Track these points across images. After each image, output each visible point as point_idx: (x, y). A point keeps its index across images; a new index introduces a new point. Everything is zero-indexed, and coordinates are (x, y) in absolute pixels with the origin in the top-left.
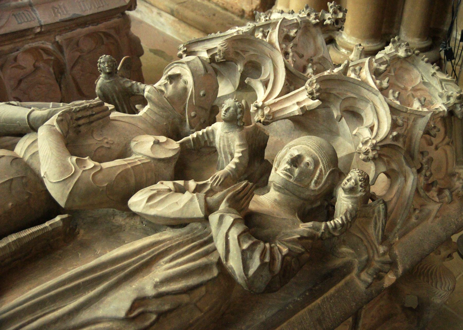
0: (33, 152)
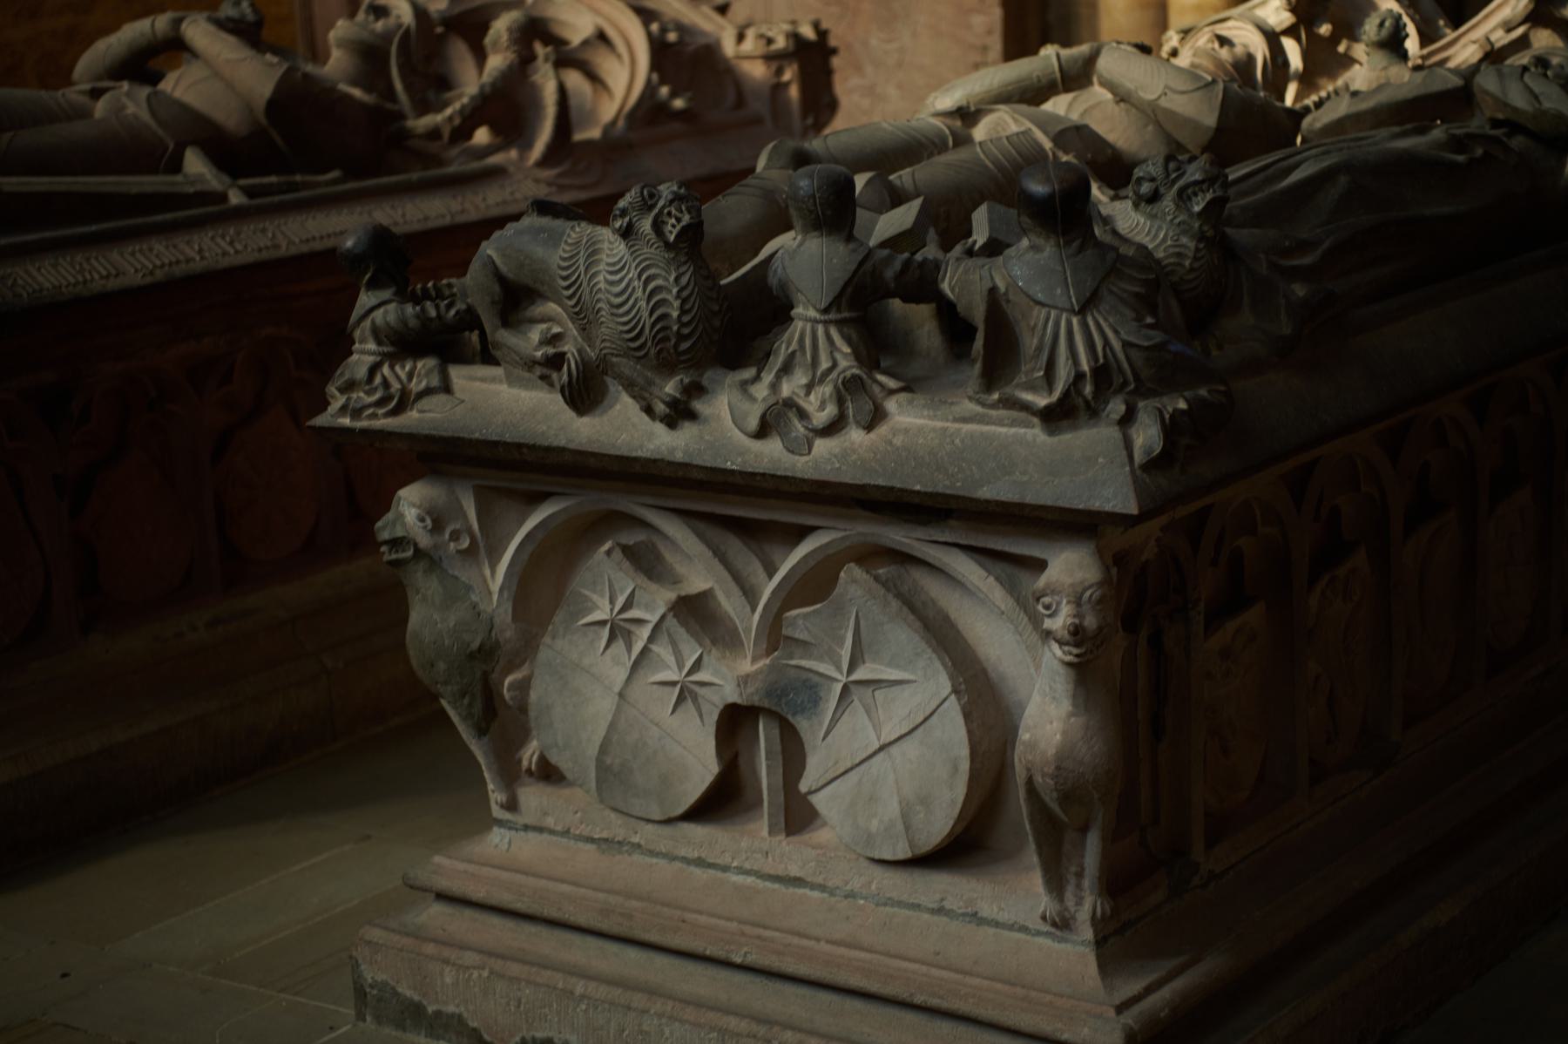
0: (1085, 106)
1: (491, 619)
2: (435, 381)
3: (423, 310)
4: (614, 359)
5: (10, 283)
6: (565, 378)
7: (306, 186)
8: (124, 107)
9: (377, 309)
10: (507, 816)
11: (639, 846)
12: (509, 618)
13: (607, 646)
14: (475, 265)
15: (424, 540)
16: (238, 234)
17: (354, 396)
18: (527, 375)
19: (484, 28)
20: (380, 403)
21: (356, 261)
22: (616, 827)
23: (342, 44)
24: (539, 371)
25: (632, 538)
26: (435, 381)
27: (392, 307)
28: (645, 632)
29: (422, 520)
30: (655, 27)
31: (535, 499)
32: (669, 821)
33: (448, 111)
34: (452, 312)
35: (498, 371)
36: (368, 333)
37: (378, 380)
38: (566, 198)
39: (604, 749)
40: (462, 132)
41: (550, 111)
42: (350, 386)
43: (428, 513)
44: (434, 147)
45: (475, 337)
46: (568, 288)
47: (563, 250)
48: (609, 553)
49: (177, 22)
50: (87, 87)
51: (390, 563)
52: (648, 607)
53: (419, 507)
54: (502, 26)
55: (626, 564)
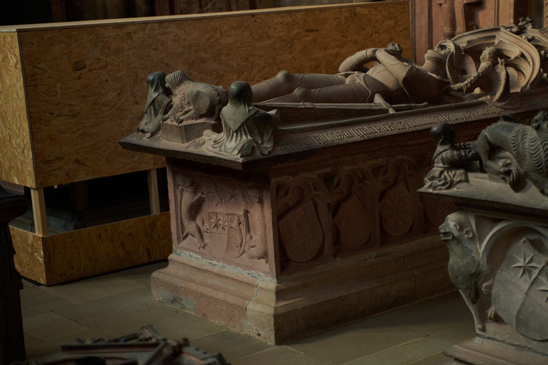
1: (479, 263)
2: (463, 178)
3: (460, 153)
4: (531, 173)
5: (318, 138)
6: (511, 179)
7: (415, 107)
8: (356, 80)
9: (443, 152)
10: (481, 333)
11: (531, 349)
12: (486, 263)
13: (522, 276)
14: (480, 137)
15: (456, 233)
16: (392, 124)
17: (434, 182)
18: (496, 177)
19: (481, 52)
20: (443, 185)
21: (437, 135)
22: (522, 341)
23: (429, 58)
24: (501, 176)
25: (533, 237)
26: (463, 178)
27: (449, 151)
28: (537, 272)
29: (456, 226)
30: (542, 52)
31: (497, 221)
32: (543, 341)
33: (466, 82)
34: (470, 154)
35: (486, 175)
36: (440, 160)
37: (443, 177)
38: (507, 113)
39: (519, 312)
40: (470, 89)
41: (503, 82)
42: (433, 178)
43: (458, 224)
44: (459, 94)
45: (478, 163)
46: (514, 147)
47: (513, 134)
48: (524, 242)
49: (375, 51)
50: (344, 73)
51: (444, 241)
52: (538, 263)
53: (455, 222)
54: (486, 52)
55: (531, 247)
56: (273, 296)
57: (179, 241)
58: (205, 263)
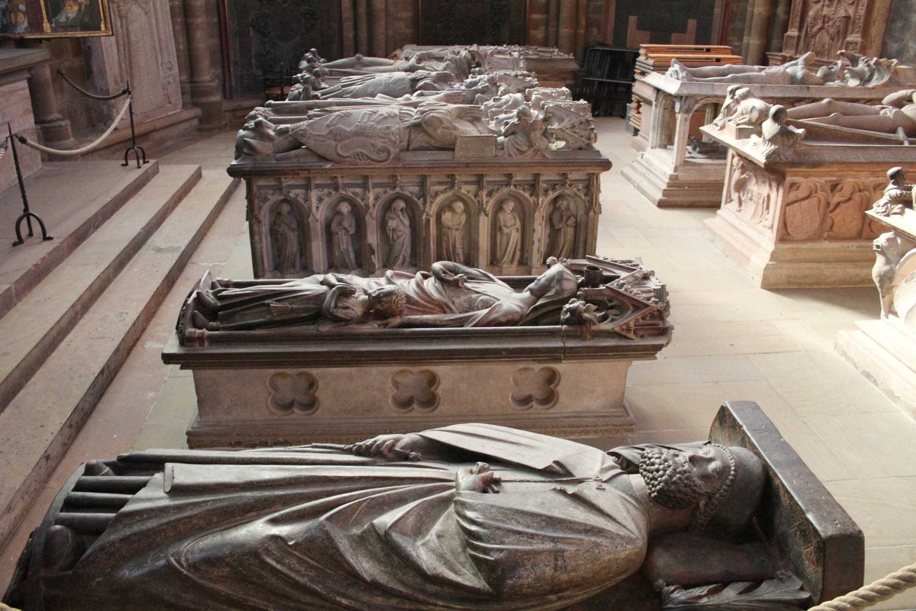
42: (879, 206)
56: (769, 257)
57: (726, 203)
58: (737, 223)
